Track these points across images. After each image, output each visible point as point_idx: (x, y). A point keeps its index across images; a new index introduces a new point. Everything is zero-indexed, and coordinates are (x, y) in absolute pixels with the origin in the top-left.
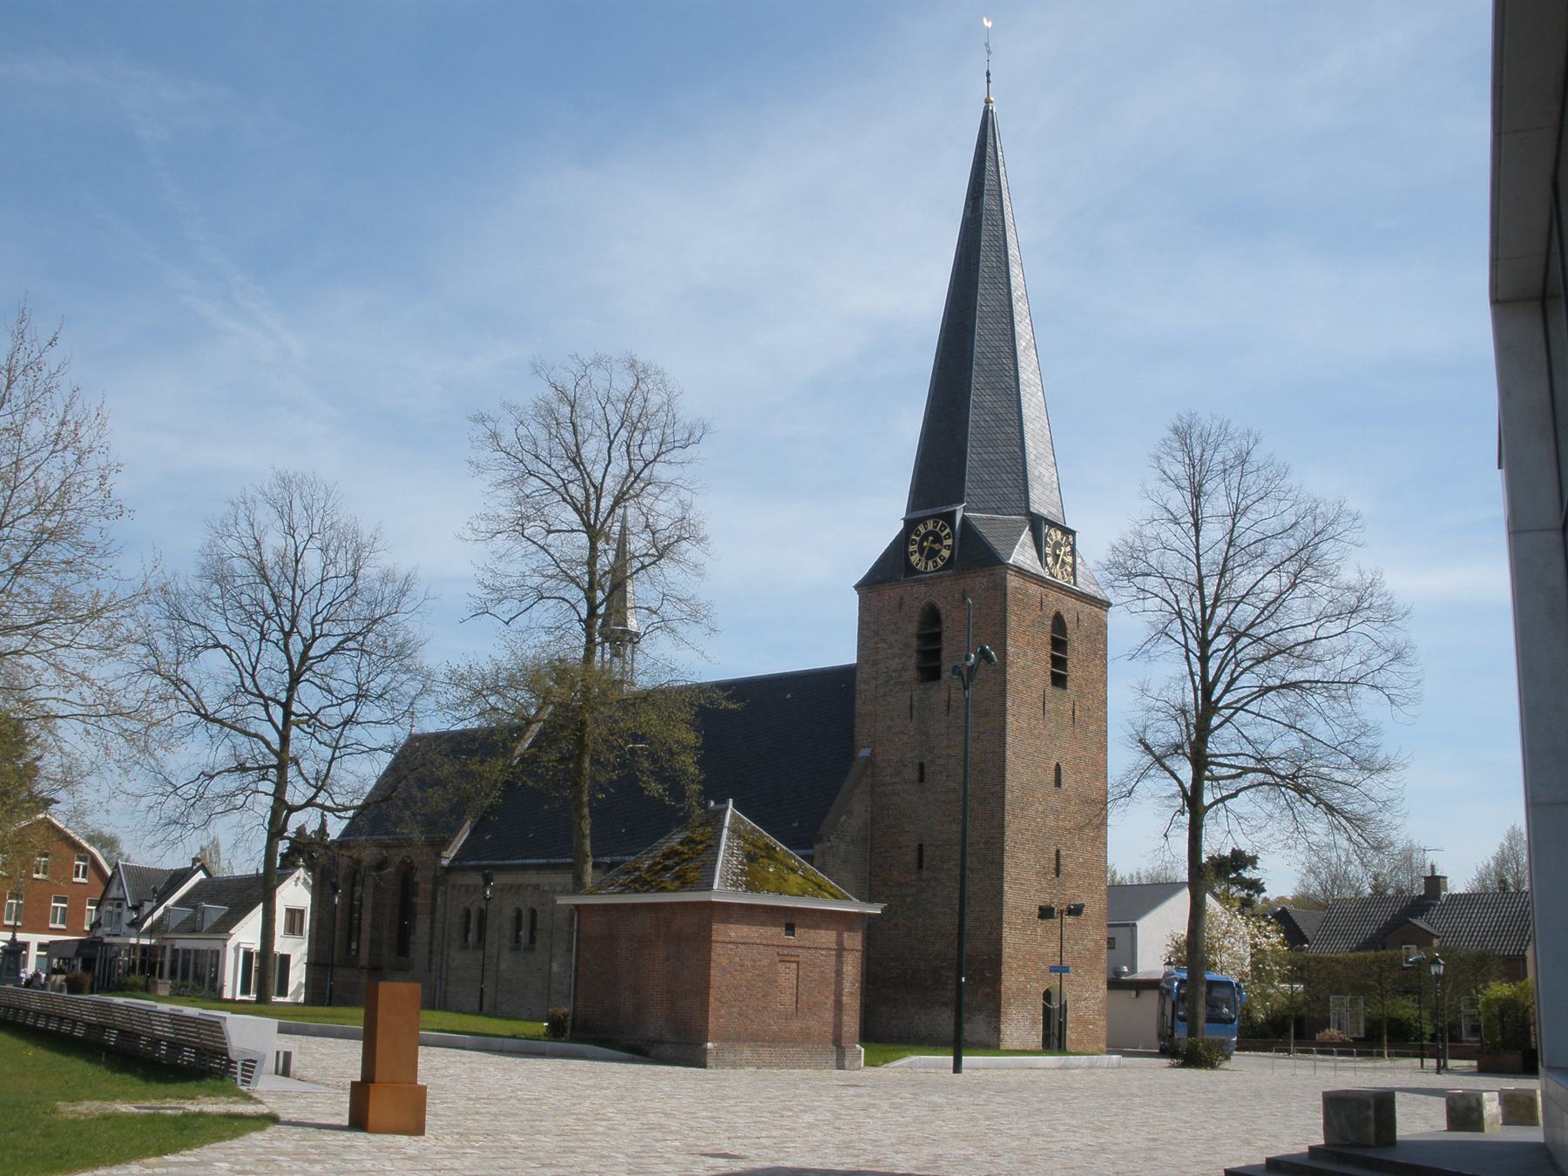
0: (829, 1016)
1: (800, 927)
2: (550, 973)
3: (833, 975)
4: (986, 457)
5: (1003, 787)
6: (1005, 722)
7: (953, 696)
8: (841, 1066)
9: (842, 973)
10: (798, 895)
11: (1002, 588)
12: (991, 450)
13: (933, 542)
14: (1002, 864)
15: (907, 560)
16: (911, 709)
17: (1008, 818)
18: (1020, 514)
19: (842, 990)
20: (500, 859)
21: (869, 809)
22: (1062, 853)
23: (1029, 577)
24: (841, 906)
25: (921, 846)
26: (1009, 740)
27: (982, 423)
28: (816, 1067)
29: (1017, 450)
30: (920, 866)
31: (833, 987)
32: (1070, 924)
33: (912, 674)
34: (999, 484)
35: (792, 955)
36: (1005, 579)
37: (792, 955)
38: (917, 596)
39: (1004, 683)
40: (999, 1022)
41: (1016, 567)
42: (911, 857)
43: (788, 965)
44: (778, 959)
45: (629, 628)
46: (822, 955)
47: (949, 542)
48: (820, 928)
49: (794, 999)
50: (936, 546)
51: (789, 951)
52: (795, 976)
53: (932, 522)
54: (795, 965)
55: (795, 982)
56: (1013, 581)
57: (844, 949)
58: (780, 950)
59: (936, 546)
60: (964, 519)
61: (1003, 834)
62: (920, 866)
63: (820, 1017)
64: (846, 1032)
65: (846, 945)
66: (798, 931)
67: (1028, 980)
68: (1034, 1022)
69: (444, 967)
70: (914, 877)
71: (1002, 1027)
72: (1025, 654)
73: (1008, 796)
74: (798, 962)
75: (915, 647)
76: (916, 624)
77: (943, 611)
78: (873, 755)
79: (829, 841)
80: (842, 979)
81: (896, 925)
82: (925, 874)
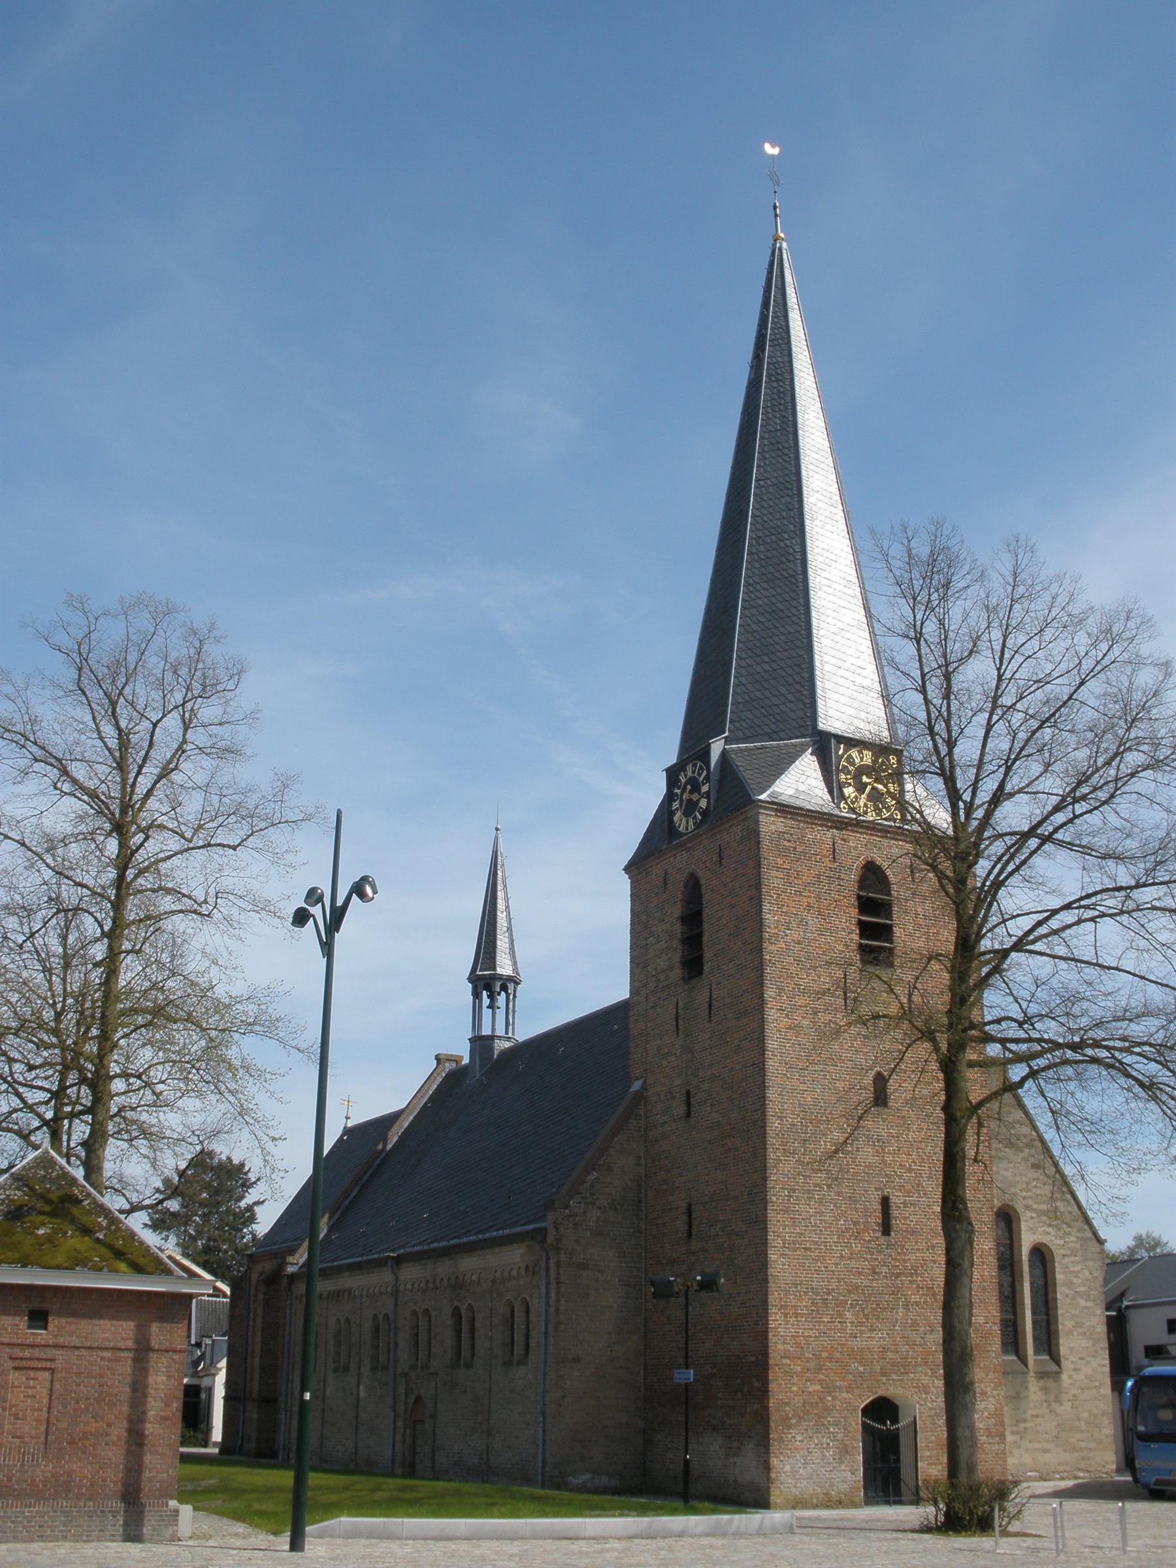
0: (115, 1455)
1: (59, 1314)
2: (358, 1398)
3: (127, 1389)
4: (759, 669)
5: (764, 1113)
6: (763, 1020)
7: (714, 994)
8: (133, 1534)
9: (146, 1386)
10: (67, 1268)
11: (753, 835)
12: (765, 658)
13: (691, 792)
14: (764, 1221)
15: (671, 821)
16: (677, 1018)
17: (771, 1156)
18: (804, 736)
19: (144, 1413)
20: (345, 1259)
21: (643, 1161)
22: (893, 1200)
23: (805, 816)
24: (152, 1283)
25: (689, 1206)
26: (772, 1044)
27: (754, 627)
28: (78, 1538)
29: (801, 652)
30: (690, 1235)
31: (125, 1408)
32: (917, 1303)
33: (678, 972)
34: (776, 701)
35: (39, 1359)
36: (757, 822)
37: (39, 1359)
38: (678, 864)
39: (760, 967)
40: (767, 1453)
41: (773, 803)
42: (681, 1223)
43: (32, 1373)
44: (11, 1364)
45: (499, 971)
46: (102, 1359)
47: (705, 788)
48: (101, 1317)
49: (43, 1428)
50: (695, 797)
51: (36, 1353)
52: (45, 1392)
53: (691, 765)
54: (47, 1374)
55: (45, 1401)
56: (769, 824)
57: (149, 1349)
58: (17, 1352)
59: (695, 797)
60: (724, 754)
61: (765, 1179)
62: (690, 1235)
63: (94, 1456)
64: (150, 1479)
65: (155, 1344)
66: (53, 1322)
67: (829, 1389)
68: (844, 1451)
69: (289, 1396)
70: (683, 1250)
71: (774, 1461)
72: (802, 922)
73: (773, 1124)
74: (52, 1371)
75: (679, 935)
76: (679, 905)
77: (703, 881)
78: (644, 1087)
79: (567, 1207)
80: (145, 1395)
81: (669, 1318)
82: (695, 1245)
